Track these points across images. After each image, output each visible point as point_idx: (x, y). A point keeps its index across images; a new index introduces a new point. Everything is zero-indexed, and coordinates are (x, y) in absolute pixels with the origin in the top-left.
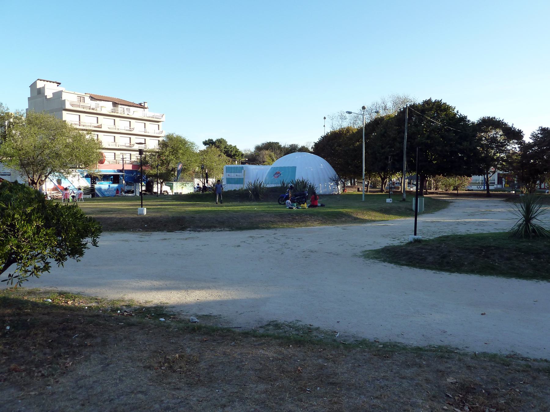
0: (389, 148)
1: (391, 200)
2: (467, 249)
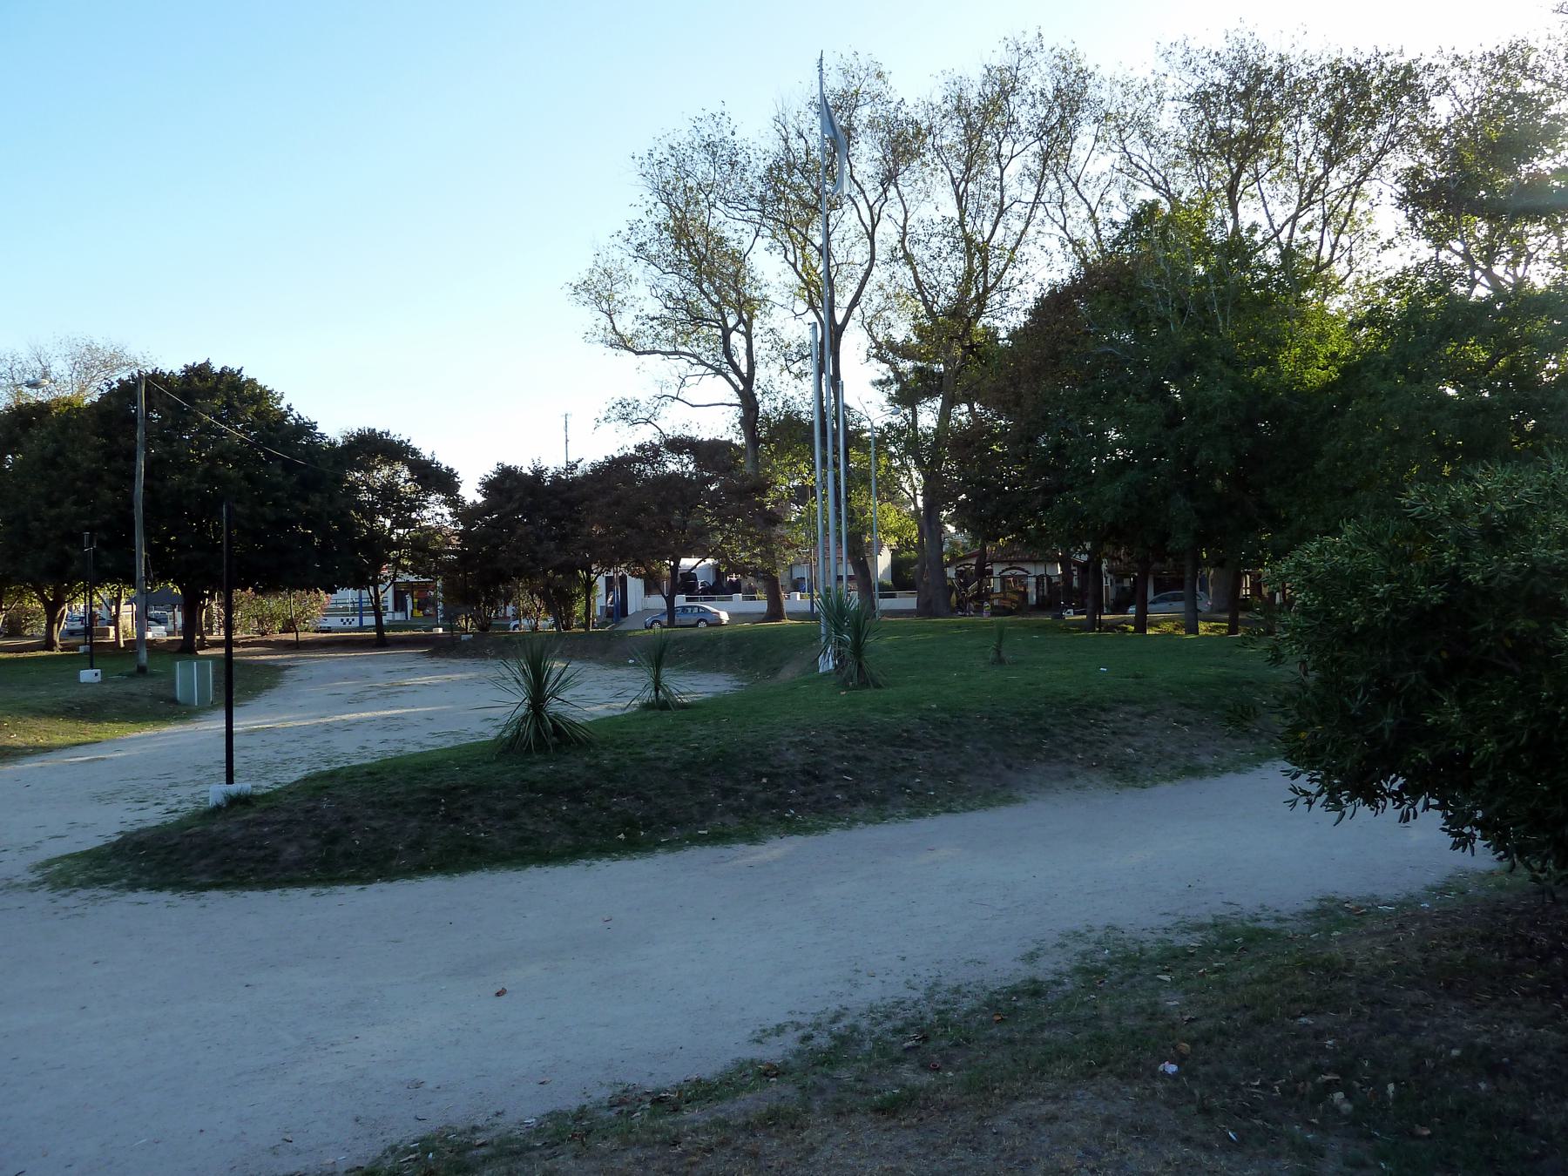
0: (75, 503)
1: (96, 675)
2: (396, 805)
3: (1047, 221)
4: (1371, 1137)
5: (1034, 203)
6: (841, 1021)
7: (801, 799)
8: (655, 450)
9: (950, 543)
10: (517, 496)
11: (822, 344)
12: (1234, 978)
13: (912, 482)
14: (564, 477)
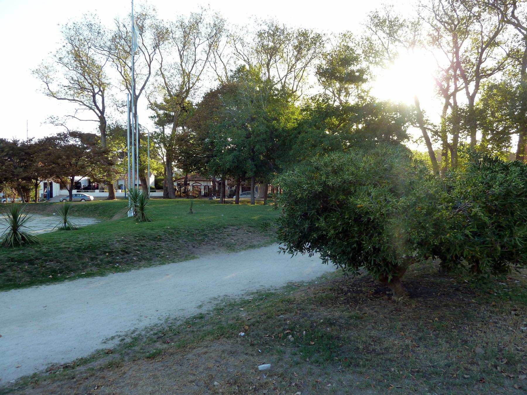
3: (210, 67)
4: (298, 347)
5: (206, 61)
6: (135, 333)
7: (121, 260)
8: (65, 136)
9: (175, 174)
10: (6, 150)
11: (131, 102)
12: (262, 307)
13: (162, 152)
14: (26, 144)
